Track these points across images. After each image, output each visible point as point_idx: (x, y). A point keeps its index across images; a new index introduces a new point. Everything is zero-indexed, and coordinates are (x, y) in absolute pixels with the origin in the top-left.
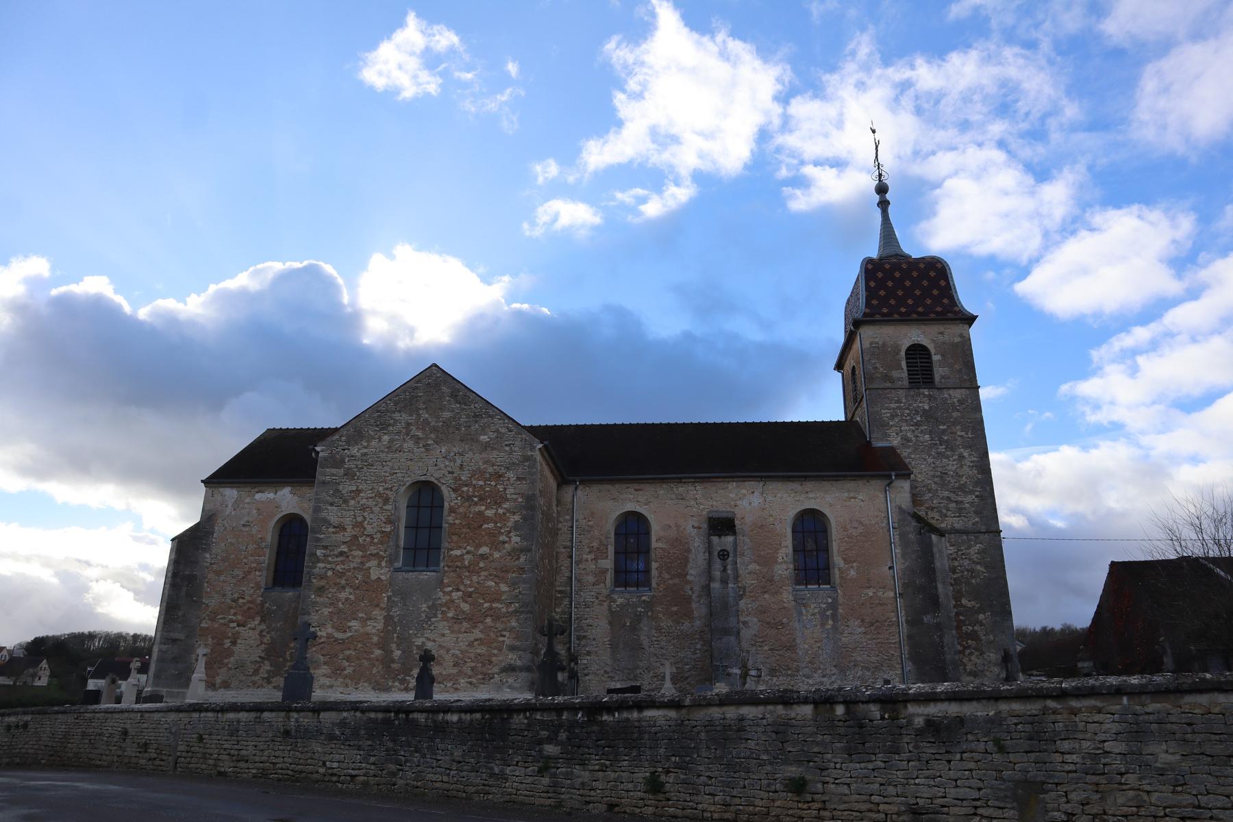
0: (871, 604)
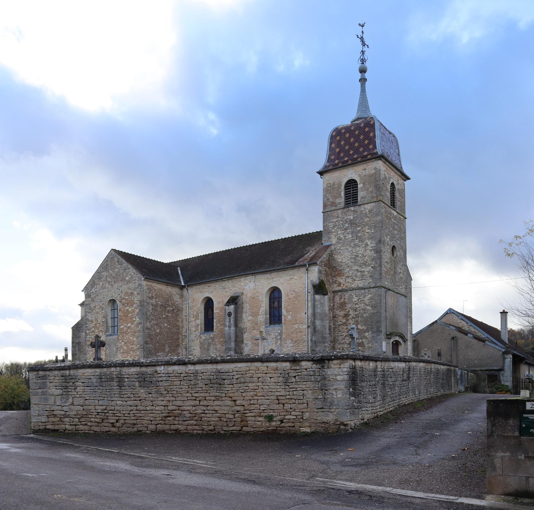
0: (296, 332)
